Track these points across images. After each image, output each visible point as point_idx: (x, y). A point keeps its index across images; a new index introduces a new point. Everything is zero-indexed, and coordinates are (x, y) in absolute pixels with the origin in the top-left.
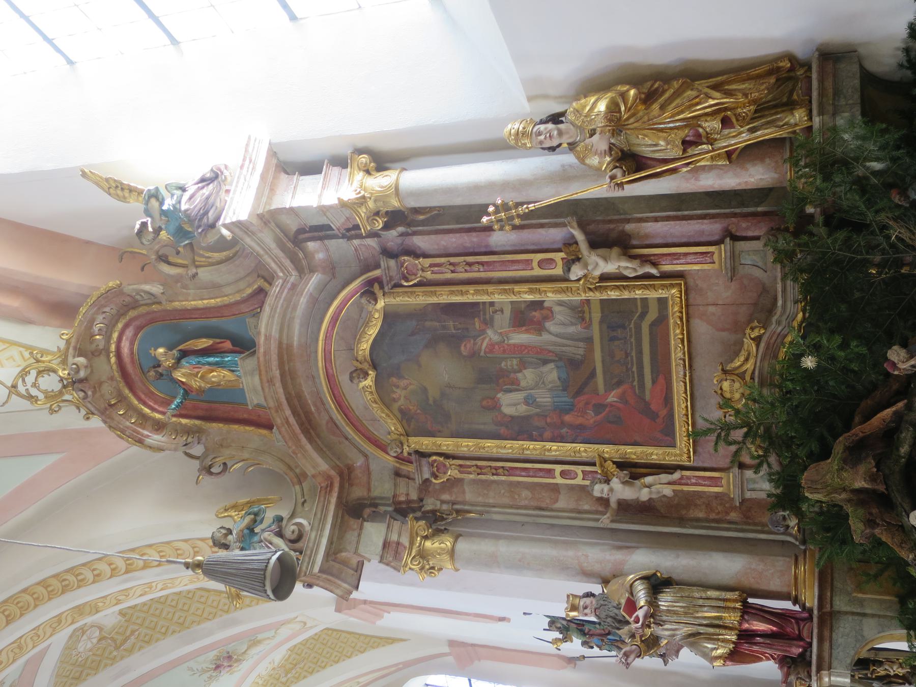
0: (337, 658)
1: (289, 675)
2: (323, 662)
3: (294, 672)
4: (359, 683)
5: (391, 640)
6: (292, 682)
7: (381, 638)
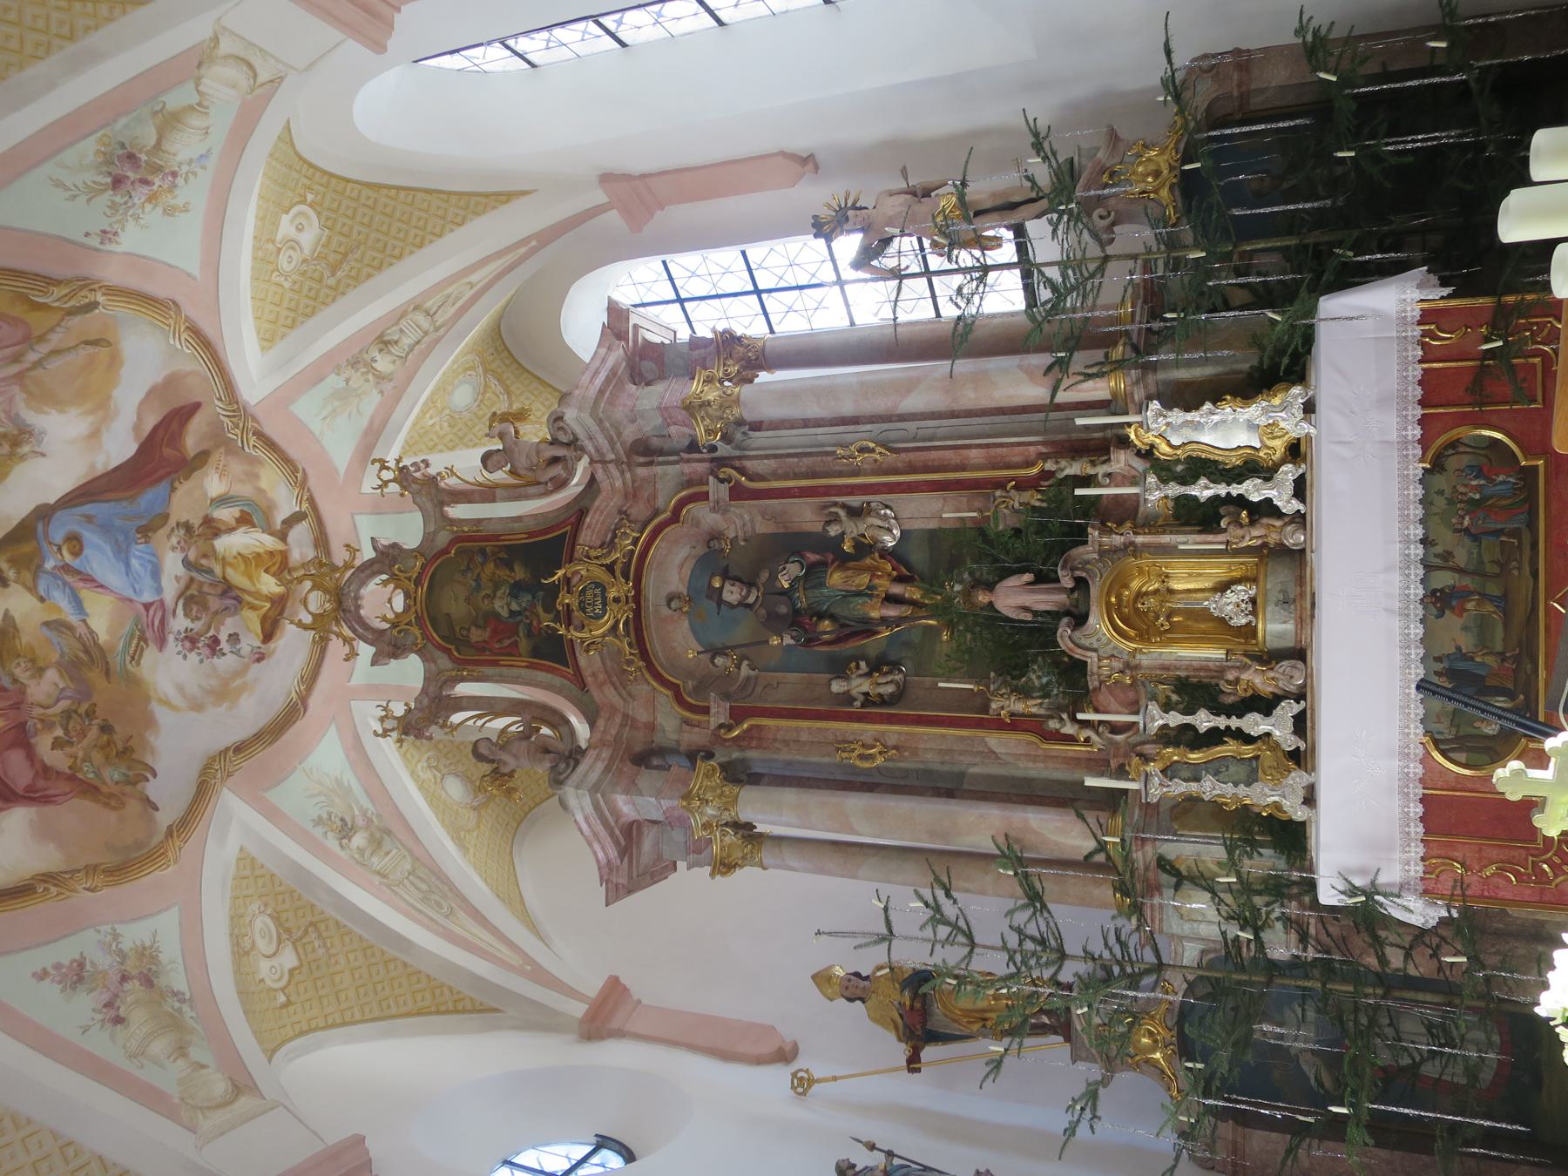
0: (418, 239)
1: (339, 274)
2: (394, 247)
3: (346, 267)
4: (472, 285)
5: (506, 197)
6: (348, 285)
7: (486, 195)
